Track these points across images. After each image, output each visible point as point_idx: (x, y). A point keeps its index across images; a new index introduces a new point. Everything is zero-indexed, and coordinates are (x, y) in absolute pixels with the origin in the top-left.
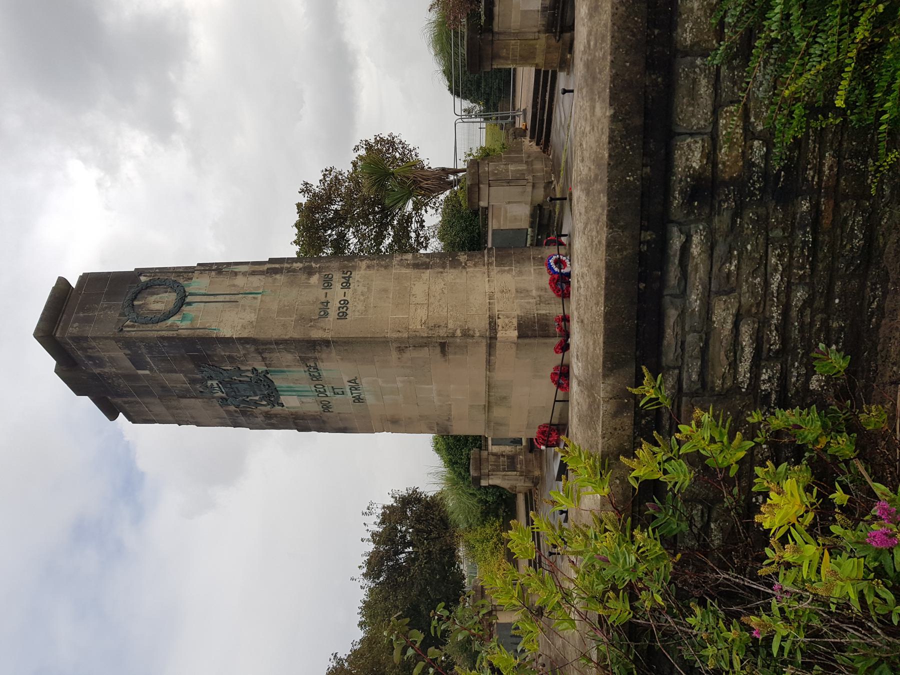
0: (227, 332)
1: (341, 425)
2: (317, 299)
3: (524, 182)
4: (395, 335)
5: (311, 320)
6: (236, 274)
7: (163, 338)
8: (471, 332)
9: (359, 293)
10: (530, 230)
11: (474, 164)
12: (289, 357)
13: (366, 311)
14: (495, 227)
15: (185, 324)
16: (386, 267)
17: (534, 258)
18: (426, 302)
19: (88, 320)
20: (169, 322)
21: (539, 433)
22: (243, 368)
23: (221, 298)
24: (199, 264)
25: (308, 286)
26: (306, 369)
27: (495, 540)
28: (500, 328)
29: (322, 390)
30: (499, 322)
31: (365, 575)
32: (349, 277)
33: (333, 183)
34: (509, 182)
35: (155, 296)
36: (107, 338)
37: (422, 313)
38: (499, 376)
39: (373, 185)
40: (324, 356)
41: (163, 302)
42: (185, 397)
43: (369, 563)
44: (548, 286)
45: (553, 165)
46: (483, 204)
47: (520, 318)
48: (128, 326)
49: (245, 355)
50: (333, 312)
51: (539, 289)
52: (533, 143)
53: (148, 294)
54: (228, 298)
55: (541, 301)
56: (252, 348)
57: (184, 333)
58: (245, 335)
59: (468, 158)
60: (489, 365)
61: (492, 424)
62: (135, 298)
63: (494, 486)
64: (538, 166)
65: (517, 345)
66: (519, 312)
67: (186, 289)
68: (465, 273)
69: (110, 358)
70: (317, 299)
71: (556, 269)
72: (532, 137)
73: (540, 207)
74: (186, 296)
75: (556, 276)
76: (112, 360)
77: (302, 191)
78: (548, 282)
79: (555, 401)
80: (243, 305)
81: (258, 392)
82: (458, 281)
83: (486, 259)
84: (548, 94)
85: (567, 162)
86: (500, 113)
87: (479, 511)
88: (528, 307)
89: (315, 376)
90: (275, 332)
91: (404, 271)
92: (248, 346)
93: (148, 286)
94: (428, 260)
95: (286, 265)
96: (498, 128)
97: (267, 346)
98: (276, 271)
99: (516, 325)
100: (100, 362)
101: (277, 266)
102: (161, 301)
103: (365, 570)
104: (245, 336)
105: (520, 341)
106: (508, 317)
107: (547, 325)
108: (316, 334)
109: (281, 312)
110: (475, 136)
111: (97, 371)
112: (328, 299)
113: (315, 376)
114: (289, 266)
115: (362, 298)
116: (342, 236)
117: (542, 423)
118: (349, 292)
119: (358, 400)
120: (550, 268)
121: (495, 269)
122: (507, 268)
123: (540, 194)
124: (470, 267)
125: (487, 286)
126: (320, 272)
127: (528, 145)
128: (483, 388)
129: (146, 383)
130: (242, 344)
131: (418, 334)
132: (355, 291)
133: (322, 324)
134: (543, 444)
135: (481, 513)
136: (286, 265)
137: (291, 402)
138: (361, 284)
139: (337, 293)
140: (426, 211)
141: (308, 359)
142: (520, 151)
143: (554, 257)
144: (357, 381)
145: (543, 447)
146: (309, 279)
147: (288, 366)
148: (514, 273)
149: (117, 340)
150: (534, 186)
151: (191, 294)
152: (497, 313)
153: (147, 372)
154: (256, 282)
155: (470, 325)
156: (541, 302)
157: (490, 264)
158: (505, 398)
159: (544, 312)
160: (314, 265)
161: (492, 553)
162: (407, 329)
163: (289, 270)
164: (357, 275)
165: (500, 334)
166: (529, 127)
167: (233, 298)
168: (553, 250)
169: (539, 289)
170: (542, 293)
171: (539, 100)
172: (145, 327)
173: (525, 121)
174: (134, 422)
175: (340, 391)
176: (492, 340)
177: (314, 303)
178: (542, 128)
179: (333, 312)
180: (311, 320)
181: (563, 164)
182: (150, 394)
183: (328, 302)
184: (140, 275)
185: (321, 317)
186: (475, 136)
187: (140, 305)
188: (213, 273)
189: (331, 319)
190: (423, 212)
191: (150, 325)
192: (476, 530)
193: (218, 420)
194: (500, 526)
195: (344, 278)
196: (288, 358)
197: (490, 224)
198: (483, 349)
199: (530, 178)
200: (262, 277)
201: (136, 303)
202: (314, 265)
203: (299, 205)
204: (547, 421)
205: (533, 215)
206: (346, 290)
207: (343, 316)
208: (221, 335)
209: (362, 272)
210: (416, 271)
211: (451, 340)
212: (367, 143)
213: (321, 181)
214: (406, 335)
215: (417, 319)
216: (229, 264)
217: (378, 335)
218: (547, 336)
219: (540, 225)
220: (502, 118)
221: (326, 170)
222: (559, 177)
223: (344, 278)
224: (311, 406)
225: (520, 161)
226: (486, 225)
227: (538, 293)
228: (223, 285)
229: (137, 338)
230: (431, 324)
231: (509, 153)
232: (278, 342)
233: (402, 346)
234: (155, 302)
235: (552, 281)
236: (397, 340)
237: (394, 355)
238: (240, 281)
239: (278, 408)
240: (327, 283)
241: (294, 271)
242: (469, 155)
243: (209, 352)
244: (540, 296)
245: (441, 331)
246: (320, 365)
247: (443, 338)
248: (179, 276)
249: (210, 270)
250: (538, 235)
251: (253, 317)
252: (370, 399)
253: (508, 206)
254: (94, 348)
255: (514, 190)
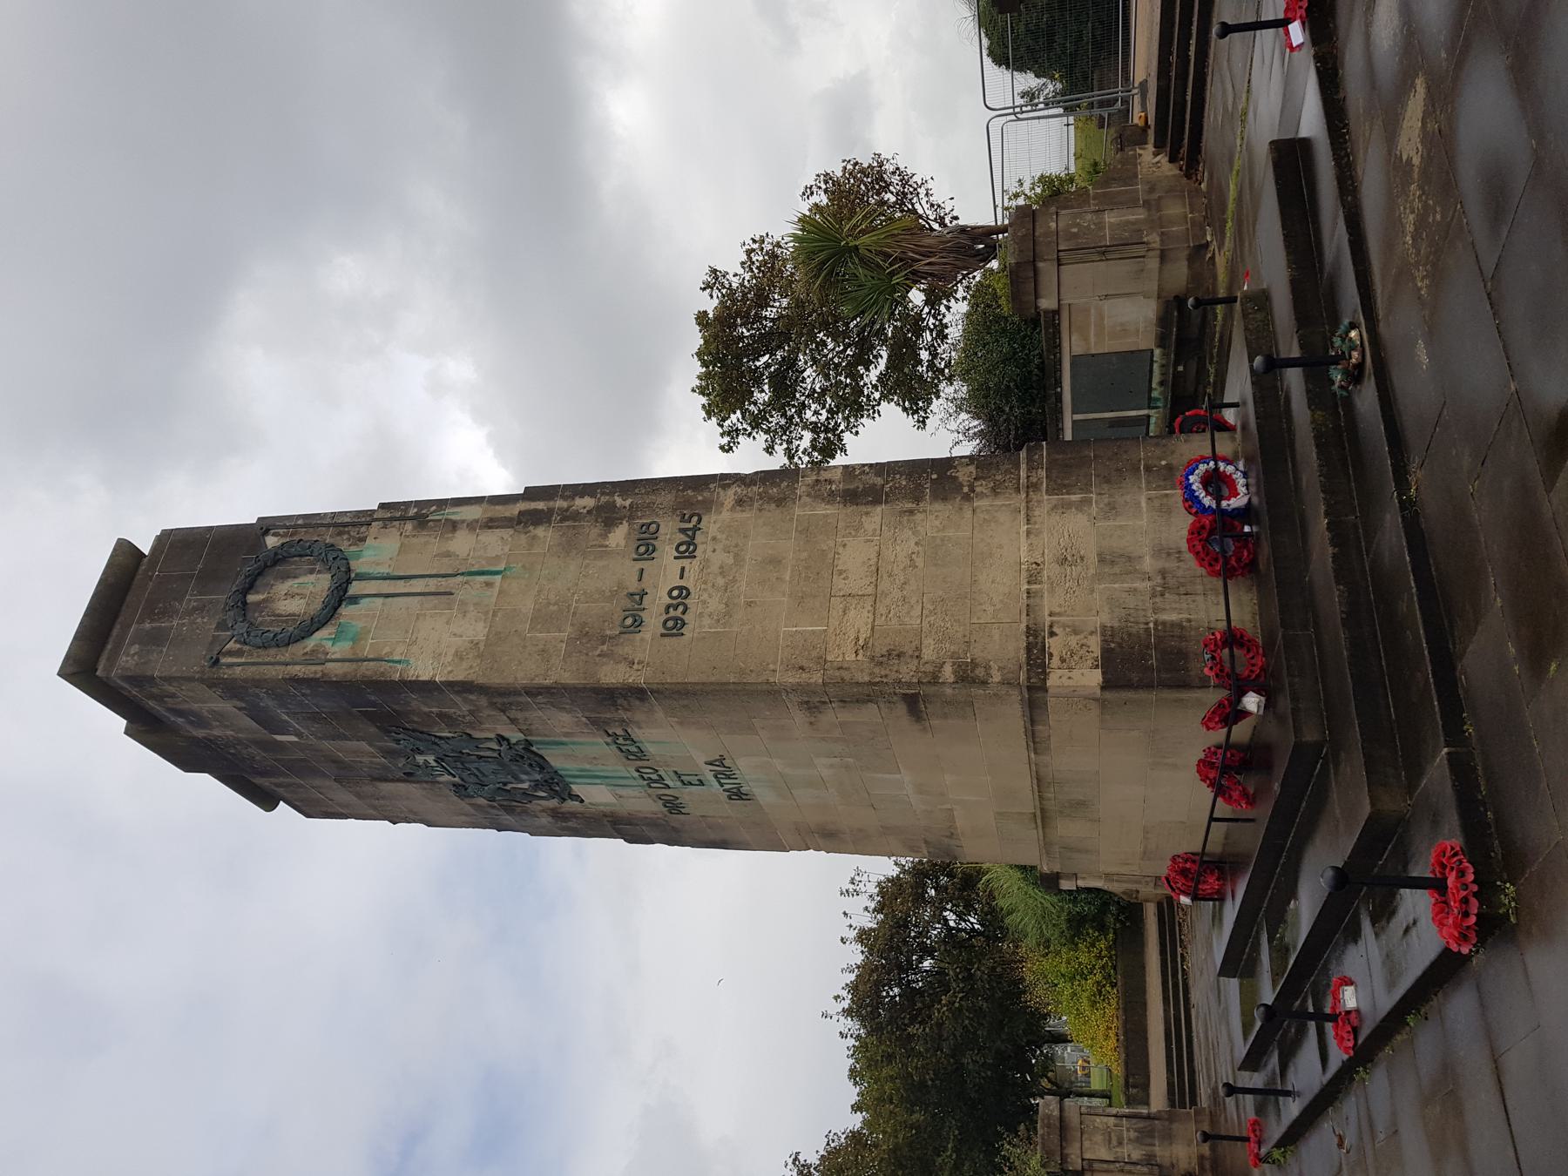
0: (423, 669)
1: (713, 836)
2: (620, 585)
3: (1141, 250)
4: (791, 678)
5: (603, 639)
6: (454, 526)
7: (296, 681)
8: (980, 672)
9: (715, 568)
10: (1157, 352)
11: (1025, 217)
12: (565, 718)
13: (728, 614)
14: (1078, 351)
15: (340, 649)
16: (780, 502)
17: (1148, 469)
18: (870, 590)
19: (156, 639)
20: (311, 643)
21: (1172, 869)
22: (476, 734)
23: (418, 586)
24: (383, 506)
25: (604, 552)
26: (609, 740)
27: (1099, 977)
28: (1055, 662)
29: (654, 777)
30: (1054, 645)
31: (848, 1012)
32: (696, 529)
33: (767, 266)
34: (1104, 253)
35: (290, 583)
36: (190, 679)
37: (859, 621)
38: (1064, 761)
39: (816, 277)
40: (639, 716)
41: (302, 596)
42: (386, 780)
43: (854, 988)
44: (1184, 546)
45: (1208, 207)
46: (1047, 303)
47: (1108, 634)
48: (230, 653)
49: (471, 712)
50: (653, 620)
51: (1161, 551)
52: (1163, 159)
53: (276, 579)
54: (432, 585)
55: (1166, 585)
56: (483, 701)
57: (336, 670)
58: (460, 676)
59: (1014, 203)
60: (1035, 741)
61: (1056, 849)
62: (250, 587)
63: (1089, 890)
64: (1174, 209)
65: (1103, 704)
66: (1105, 618)
67: (353, 564)
68: (968, 514)
69: (212, 712)
70: (620, 585)
71: (1208, 501)
72: (1159, 146)
73: (1180, 301)
74: (349, 581)
75: (1206, 521)
76: (220, 716)
77: (707, 286)
78: (1185, 533)
79: (1212, 819)
80: (462, 603)
81: (524, 777)
82: (950, 533)
83: (1023, 474)
84: (1193, 42)
85: (1239, 200)
86: (1097, 95)
87: (1064, 916)
88: (1131, 602)
89: (633, 753)
90: (521, 670)
91: (823, 510)
92: (472, 697)
93: (278, 559)
94: (879, 481)
95: (560, 503)
96: (1093, 125)
97: (511, 699)
98: (536, 518)
99: (1098, 653)
100: (200, 721)
101: (541, 505)
102: (295, 595)
103: (846, 1004)
104: (460, 678)
105: (1108, 695)
106: (1076, 632)
107: (1182, 655)
108: (613, 675)
109: (542, 618)
110: (1047, 146)
111: (200, 733)
112: (644, 585)
113: (633, 753)
114: (565, 504)
115: (721, 581)
116: (790, 363)
117: (1180, 851)
118: (692, 567)
119: (737, 794)
120: (1191, 499)
121: (1045, 501)
122: (1074, 498)
123: (1179, 274)
124: (982, 495)
125: (1024, 548)
126: (631, 518)
127: (1151, 161)
128: (1025, 784)
129: (301, 755)
130: (458, 693)
131: (847, 675)
132: (706, 563)
133: (626, 650)
134: (1186, 894)
135: (1069, 921)
136: (560, 503)
137: (596, 795)
138: (719, 547)
139: (666, 570)
140: (948, 308)
141: (607, 722)
142: (1132, 178)
143: (1202, 467)
144: (726, 763)
145: (1185, 900)
146: (605, 536)
147: (566, 735)
148: (1094, 510)
149: (212, 684)
150: (1163, 257)
151: (362, 577)
152: (1048, 620)
153: (293, 739)
154: (495, 543)
155: (977, 652)
156: (1166, 587)
157: (1032, 487)
158: (1082, 804)
159: (1173, 617)
160: (619, 501)
161: (1093, 1004)
162: (822, 661)
163: (569, 516)
164: (712, 524)
165: (1056, 679)
166: (1151, 122)
167: (444, 584)
168: (1198, 445)
169: (1161, 551)
170: (1171, 564)
171: (1174, 59)
172: (272, 654)
173: (1144, 109)
174: (308, 816)
175: (694, 779)
176: (1035, 696)
177: (614, 594)
178: (1182, 123)
179: (653, 620)
180: (603, 639)
181: (1231, 206)
182: (315, 772)
183: (643, 594)
184: (266, 532)
185: (626, 630)
186: (1047, 146)
187: (258, 604)
188: (409, 526)
189: (648, 636)
190: (943, 309)
191: (273, 651)
192: (1058, 953)
193: (463, 818)
194: (1109, 948)
195: (683, 531)
196: (561, 721)
197: (1065, 345)
198: (1013, 712)
199: (1154, 239)
200: (507, 533)
201: (251, 598)
202: (619, 501)
203: (701, 318)
204: (1197, 848)
205: (1163, 321)
206: (685, 562)
207: (675, 626)
208: (411, 675)
209: (726, 515)
210: (851, 509)
211: (932, 690)
212: (827, 177)
213: (743, 263)
214: (817, 678)
215: (848, 634)
216: (442, 504)
217: (752, 679)
218: (1185, 685)
219: (1181, 342)
220: (1102, 104)
221: (754, 241)
222: (1223, 234)
223: (683, 531)
224: (639, 801)
225: (1132, 203)
226: (1056, 346)
227: (1160, 564)
228: (426, 553)
229: (245, 680)
230: (880, 649)
231: (1106, 183)
232: (534, 692)
233: (813, 701)
234: (290, 595)
235: (1195, 532)
236: (796, 689)
237: (799, 717)
238: (462, 543)
239: (571, 805)
240: (646, 547)
241: (576, 516)
242: (1016, 196)
243: (397, 707)
244: (1163, 573)
245: (904, 669)
246: (636, 733)
247: (909, 685)
248: (340, 534)
249: (403, 519)
250: (1176, 364)
251: (476, 630)
252: (765, 796)
253: (1107, 306)
254: (173, 696)
255: (1118, 270)
